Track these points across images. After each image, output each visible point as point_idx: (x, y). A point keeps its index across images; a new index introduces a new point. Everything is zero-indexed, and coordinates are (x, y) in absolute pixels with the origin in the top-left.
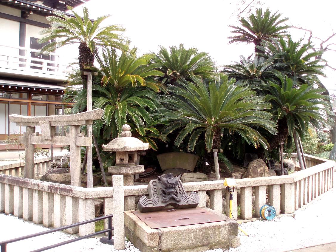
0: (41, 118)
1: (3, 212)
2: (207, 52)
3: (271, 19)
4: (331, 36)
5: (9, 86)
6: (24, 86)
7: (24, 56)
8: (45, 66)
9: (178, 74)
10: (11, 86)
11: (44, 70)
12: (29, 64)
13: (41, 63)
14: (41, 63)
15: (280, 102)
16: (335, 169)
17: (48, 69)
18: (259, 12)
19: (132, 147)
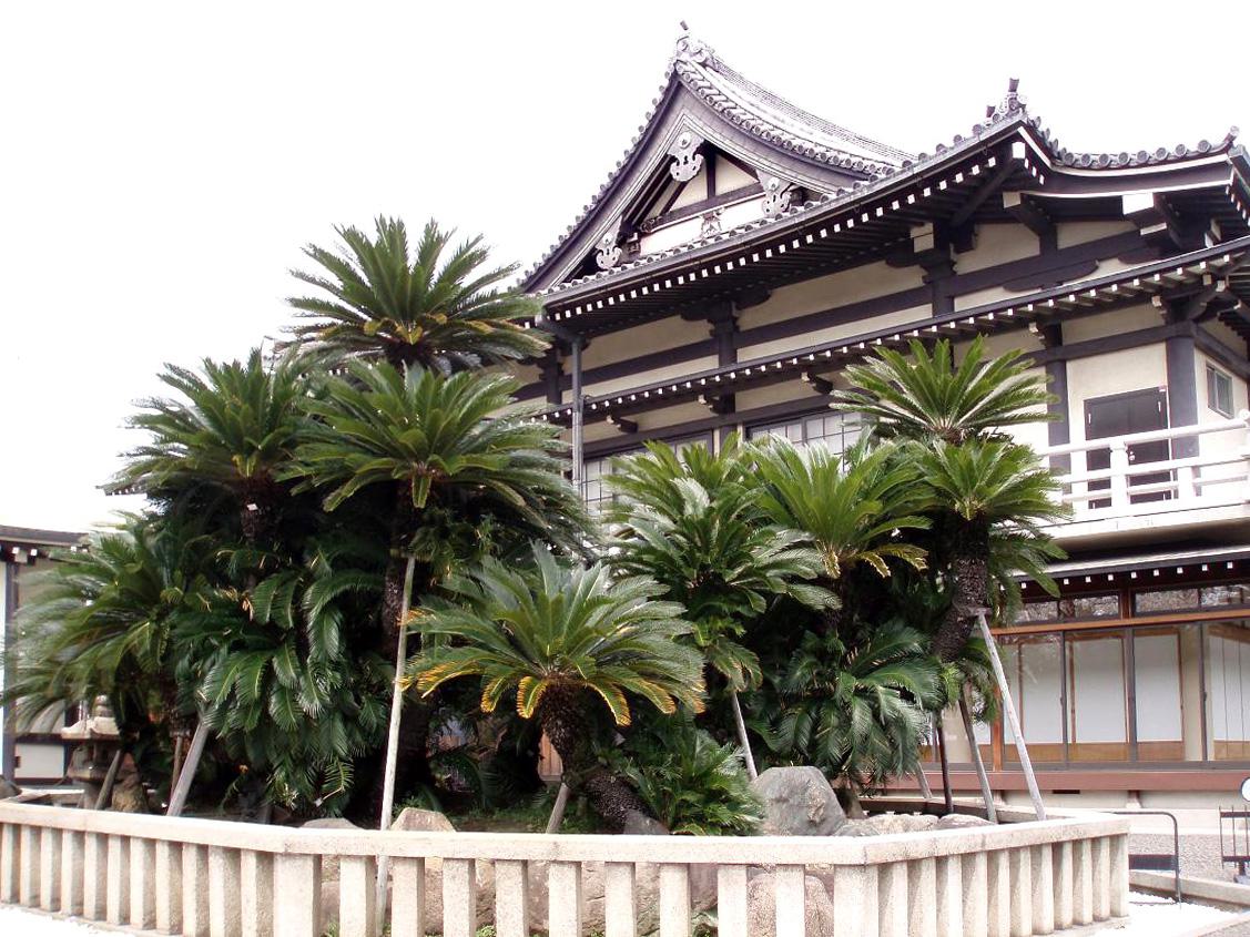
0: (174, 749)
1: (15, 898)
2: (424, 228)
3: (108, 639)
4: (1148, 906)
5: (1106, 575)
6: (1162, 566)
7: (1198, 455)
8: (1184, 482)
9: (245, 493)
10: (1160, 570)
11: (1186, 497)
12: (1119, 491)
13: (1163, 476)
14: (1163, 476)
15: (551, 630)
16: (1090, 405)
17: (1136, 499)
18: (394, 234)
19: (913, 149)
